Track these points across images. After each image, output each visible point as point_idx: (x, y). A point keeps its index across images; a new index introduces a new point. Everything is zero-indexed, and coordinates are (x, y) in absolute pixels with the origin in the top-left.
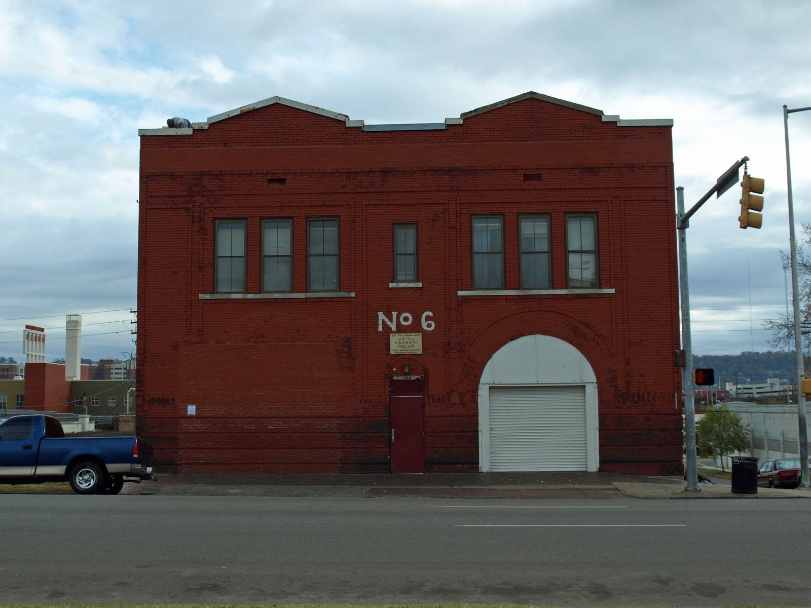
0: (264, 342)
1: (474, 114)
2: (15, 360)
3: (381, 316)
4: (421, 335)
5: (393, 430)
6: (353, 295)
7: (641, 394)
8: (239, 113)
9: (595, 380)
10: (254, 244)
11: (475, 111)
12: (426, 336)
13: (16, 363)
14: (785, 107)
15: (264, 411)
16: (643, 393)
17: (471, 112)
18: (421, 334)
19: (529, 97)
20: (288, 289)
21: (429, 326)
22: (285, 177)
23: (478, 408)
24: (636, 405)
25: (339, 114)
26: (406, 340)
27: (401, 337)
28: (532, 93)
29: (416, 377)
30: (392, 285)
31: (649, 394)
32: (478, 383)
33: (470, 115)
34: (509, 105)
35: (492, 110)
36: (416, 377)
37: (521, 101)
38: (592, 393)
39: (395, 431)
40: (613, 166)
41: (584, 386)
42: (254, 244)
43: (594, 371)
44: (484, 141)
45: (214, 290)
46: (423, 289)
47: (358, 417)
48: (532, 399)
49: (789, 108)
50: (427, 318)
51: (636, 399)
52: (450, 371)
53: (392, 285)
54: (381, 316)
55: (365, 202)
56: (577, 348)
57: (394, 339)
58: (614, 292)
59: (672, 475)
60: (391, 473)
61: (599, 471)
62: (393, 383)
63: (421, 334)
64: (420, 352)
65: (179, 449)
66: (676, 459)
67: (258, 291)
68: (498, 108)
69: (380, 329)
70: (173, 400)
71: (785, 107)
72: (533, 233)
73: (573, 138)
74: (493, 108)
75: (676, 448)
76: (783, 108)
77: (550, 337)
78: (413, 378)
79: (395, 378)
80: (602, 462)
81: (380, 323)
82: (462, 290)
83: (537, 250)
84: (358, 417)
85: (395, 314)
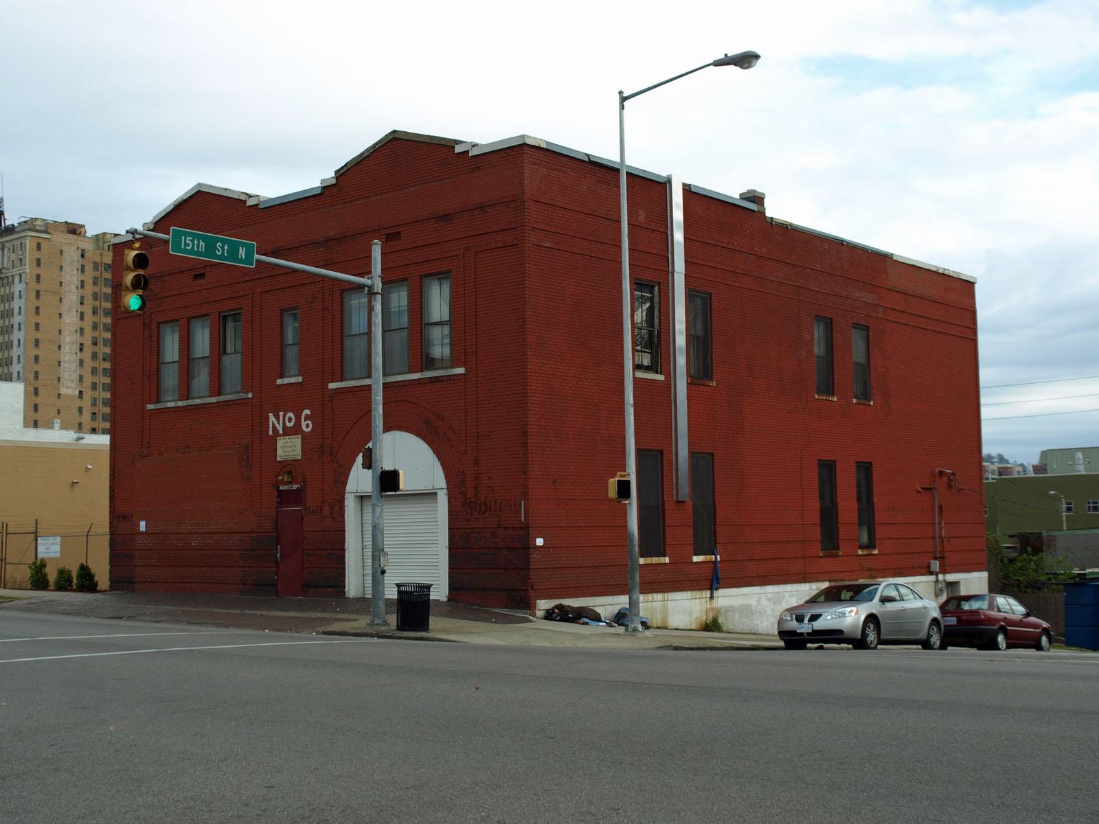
0: (189, 452)
1: (345, 169)
2: (1006, 457)
3: (272, 418)
4: (300, 438)
5: (279, 547)
6: (250, 395)
7: (488, 502)
8: (934, 269)
9: (445, 486)
10: (186, 344)
11: (346, 165)
12: (305, 438)
13: (1007, 462)
14: (621, 93)
15: (189, 526)
16: (490, 501)
17: (342, 168)
18: (300, 436)
19: (392, 137)
20: (207, 394)
21: (307, 426)
22: (204, 271)
23: (344, 521)
24: (484, 516)
25: (243, 193)
26: (289, 444)
27: (285, 441)
28: (394, 132)
29: (297, 486)
30: (279, 382)
31: (495, 502)
32: (343, 492)
33: (341, 172)
34: (374, 151)
35: (360, 162)
36: (297, 486)
37: (385, 144)
38: (443, 498)
39: (281, 548)
40: (466, 209)
41: (436, 493)
42: (186, 344)
43: (444, 470)
44: (354, 200)
45: (158, 400)
46: (304, 383)
47: (254, 532)
48: (424, 509)
49: (625, 95)
50: (307, 418)
51: (483, 509)
52: (323, 478)
53: (279, 382)
54: (272, 418)
55: (260, 290)
56: (429, 446)
57: (281, 442)
58: (664, 379)
59: (517, 609)
60: (277, 596)
61: (448, 601)
62: (280, 492)
63: (300, 436)
64: (299, 458)
65: (135, 566)
66: (523, 588)
67: (186, 398)
68: (366, 157)
69: (271, 433)
70: (132, 516)
71: (621, 93)
72: (398, 305)
73: (424, 181)
74: (361, 159)
75: (522, 574)
76: (618, 95)
77: (405, 433)
78: (295, 487)
79: (281, 488)
80: (452, 588)
81: (271, 423)
82: (333, 382)
83: (392, 329)
84: (254, 532)
85: (281, 414)
